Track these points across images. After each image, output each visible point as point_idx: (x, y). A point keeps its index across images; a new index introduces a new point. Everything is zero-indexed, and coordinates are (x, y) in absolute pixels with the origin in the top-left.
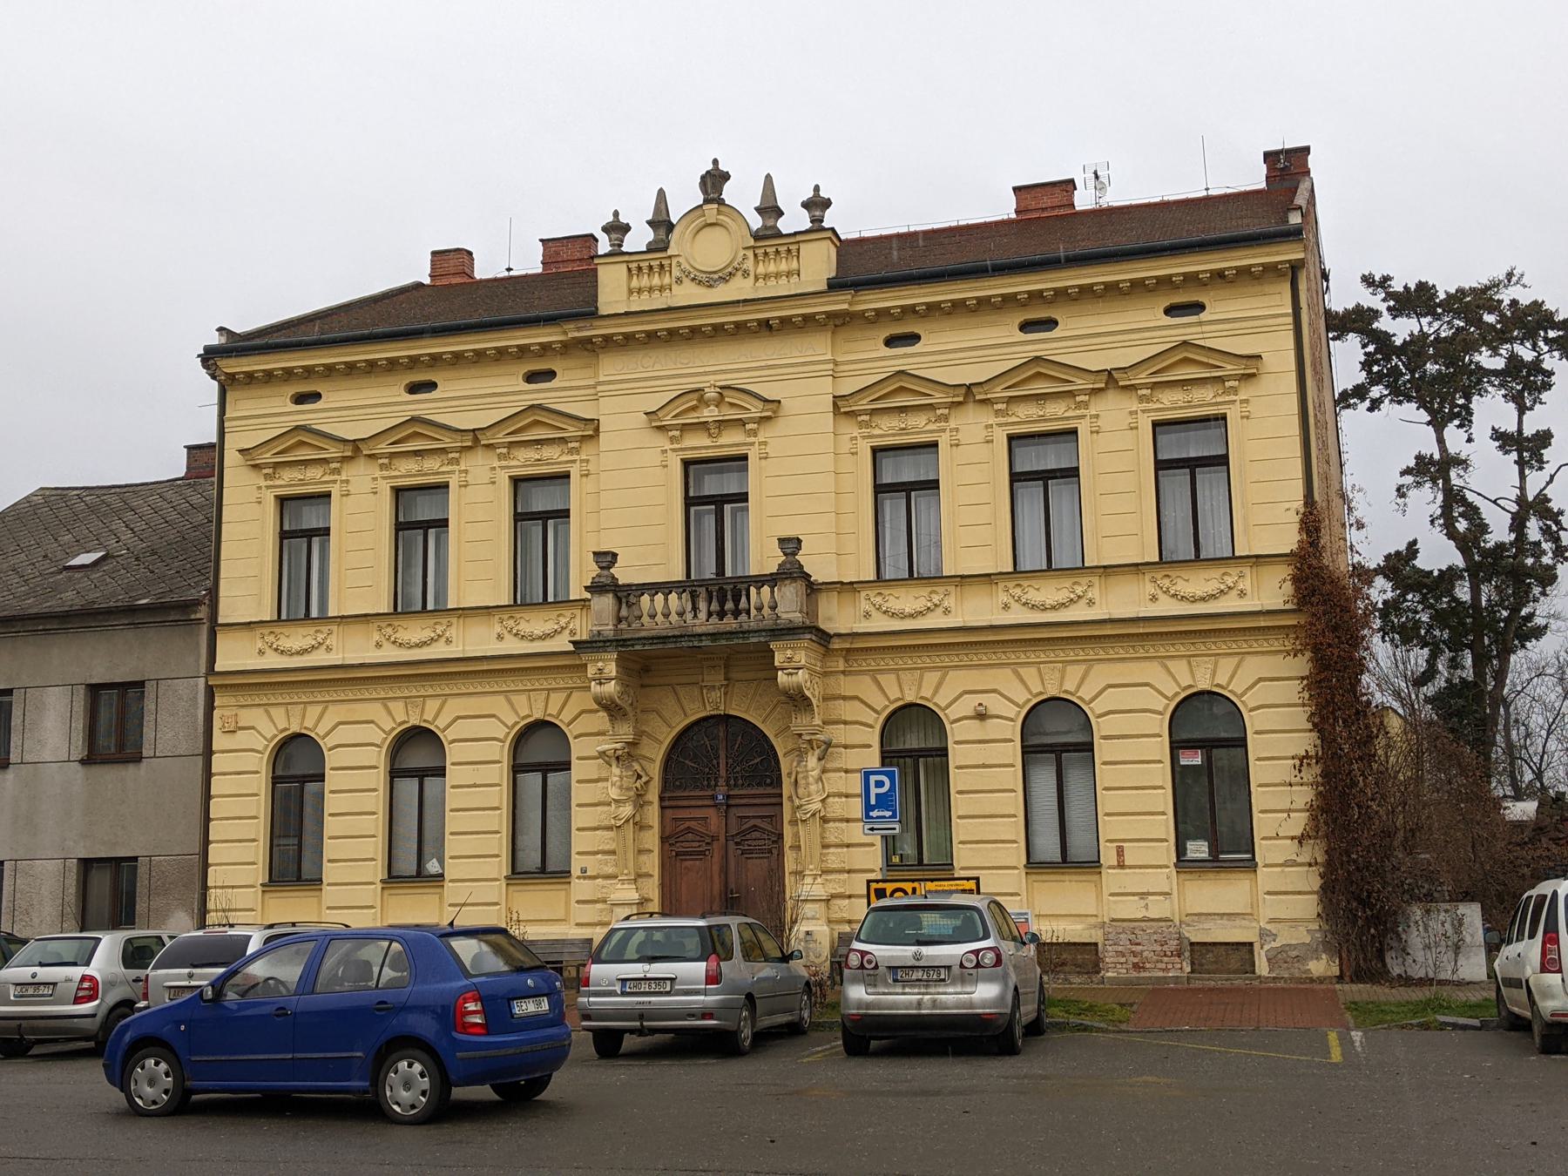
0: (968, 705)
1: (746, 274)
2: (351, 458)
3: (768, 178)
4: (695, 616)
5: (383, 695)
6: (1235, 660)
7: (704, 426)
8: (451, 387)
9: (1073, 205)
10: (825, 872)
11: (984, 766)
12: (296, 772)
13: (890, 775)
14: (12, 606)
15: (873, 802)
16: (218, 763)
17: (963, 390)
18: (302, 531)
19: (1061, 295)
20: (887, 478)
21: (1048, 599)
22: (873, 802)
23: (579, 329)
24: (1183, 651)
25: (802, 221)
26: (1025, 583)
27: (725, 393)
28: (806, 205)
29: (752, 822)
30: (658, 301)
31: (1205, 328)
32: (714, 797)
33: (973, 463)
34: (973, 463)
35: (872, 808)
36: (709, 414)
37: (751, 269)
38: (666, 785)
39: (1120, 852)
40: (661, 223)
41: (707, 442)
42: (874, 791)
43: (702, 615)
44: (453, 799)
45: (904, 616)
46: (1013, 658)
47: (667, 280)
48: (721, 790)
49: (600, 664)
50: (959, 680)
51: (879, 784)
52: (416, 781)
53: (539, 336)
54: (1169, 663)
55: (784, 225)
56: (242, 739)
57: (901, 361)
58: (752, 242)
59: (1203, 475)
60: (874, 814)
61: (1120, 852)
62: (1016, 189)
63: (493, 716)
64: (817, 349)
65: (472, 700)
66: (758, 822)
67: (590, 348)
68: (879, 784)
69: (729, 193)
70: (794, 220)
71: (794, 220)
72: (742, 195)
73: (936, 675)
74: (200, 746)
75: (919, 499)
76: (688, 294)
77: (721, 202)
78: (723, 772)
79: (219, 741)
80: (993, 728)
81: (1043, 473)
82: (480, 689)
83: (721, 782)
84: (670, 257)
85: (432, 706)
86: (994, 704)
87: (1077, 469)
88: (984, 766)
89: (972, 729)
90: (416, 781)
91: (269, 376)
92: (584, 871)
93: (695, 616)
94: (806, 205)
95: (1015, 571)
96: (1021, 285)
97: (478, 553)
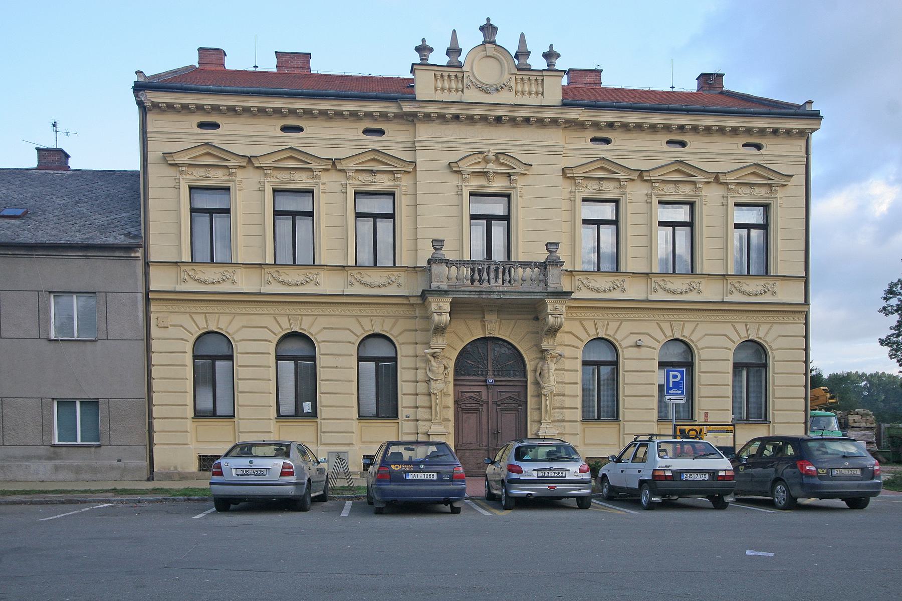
0: (633, 339)
1: (510, 89)
2: (328, 170)
3: (522, 35)
4: (496, 281)
5: (205, 310)
6: (769, 326)
7: (485, 174)
8: (229, 127)
9: (223, 65)
10: (554, 421)
11: (639, 371)
12: (212, 357)
13: (681, 372)
14: (4, 240)
15: (671, 385)
16: (155, 345)
17: (638, 173)
18: (210, 210)
19: (308, 113)
20: (198, 205)
21: (293, 281)
22: (671, 385)
23: (410, 106)
24: (742, 320)
25: (542, 64)
26: (590, 278)
27: (500, 156)
28: (418, 49)
29: (510, 395)
30: (454, 97)
31: (766, 158)
32: (486, 381)
33: (250, 201)
34: (250, 201)
35: (671, 389)
36: (491, 167)
37: (514, 87)
38: (457, 373)
39: (706, 415)
40: (453, 51)
41: (486, 184)
42: (672, 380)
43: (500, 281)
44: (240, 373)
45: (371, 286)
46: (657, 317)
47: (520, 88)
48: (494, 376)
49: (441, 304)
50: (627, 327)
51: (675, 377)
52: (293, 363)
53: (273, 103)
54: (193, 316)
55: (432, 59)
56: (172, 332)
57: (375, 144)
58: (516, 71)
59: (300, 221)
60: (671, 392)
61: (706, 415)
62: (200, 49)
63: (181, 326)
64: (556, 137)
65: (334, 319)
66: (510, 395)
67: (411, 119)
68: (675, 377)
69: (499, 39)
70: (537, 62)
71: (537, 62)
72: (507, 40)
73: (693, 325)
74: (142, 334)
75: (219, 221)
76: (472, 95)
77: (494, 42)
78: (490, 367)
79: (155, 332)
80: (644, 352)
81: (293, 211)
82: (338, 313)
83: (490, 373)
84: (463, 72)
85: (613, 325)
86: (646, 341)
87: (471, 218)
88: (639, 371)
89: (634, 352)
90: (293, 363)
91: (185, 107)
92: (407, 416)
93: (496, 281)
94: (418, 49)
95: (192, 262)
96: (674, 120)
97: (333, 228)
